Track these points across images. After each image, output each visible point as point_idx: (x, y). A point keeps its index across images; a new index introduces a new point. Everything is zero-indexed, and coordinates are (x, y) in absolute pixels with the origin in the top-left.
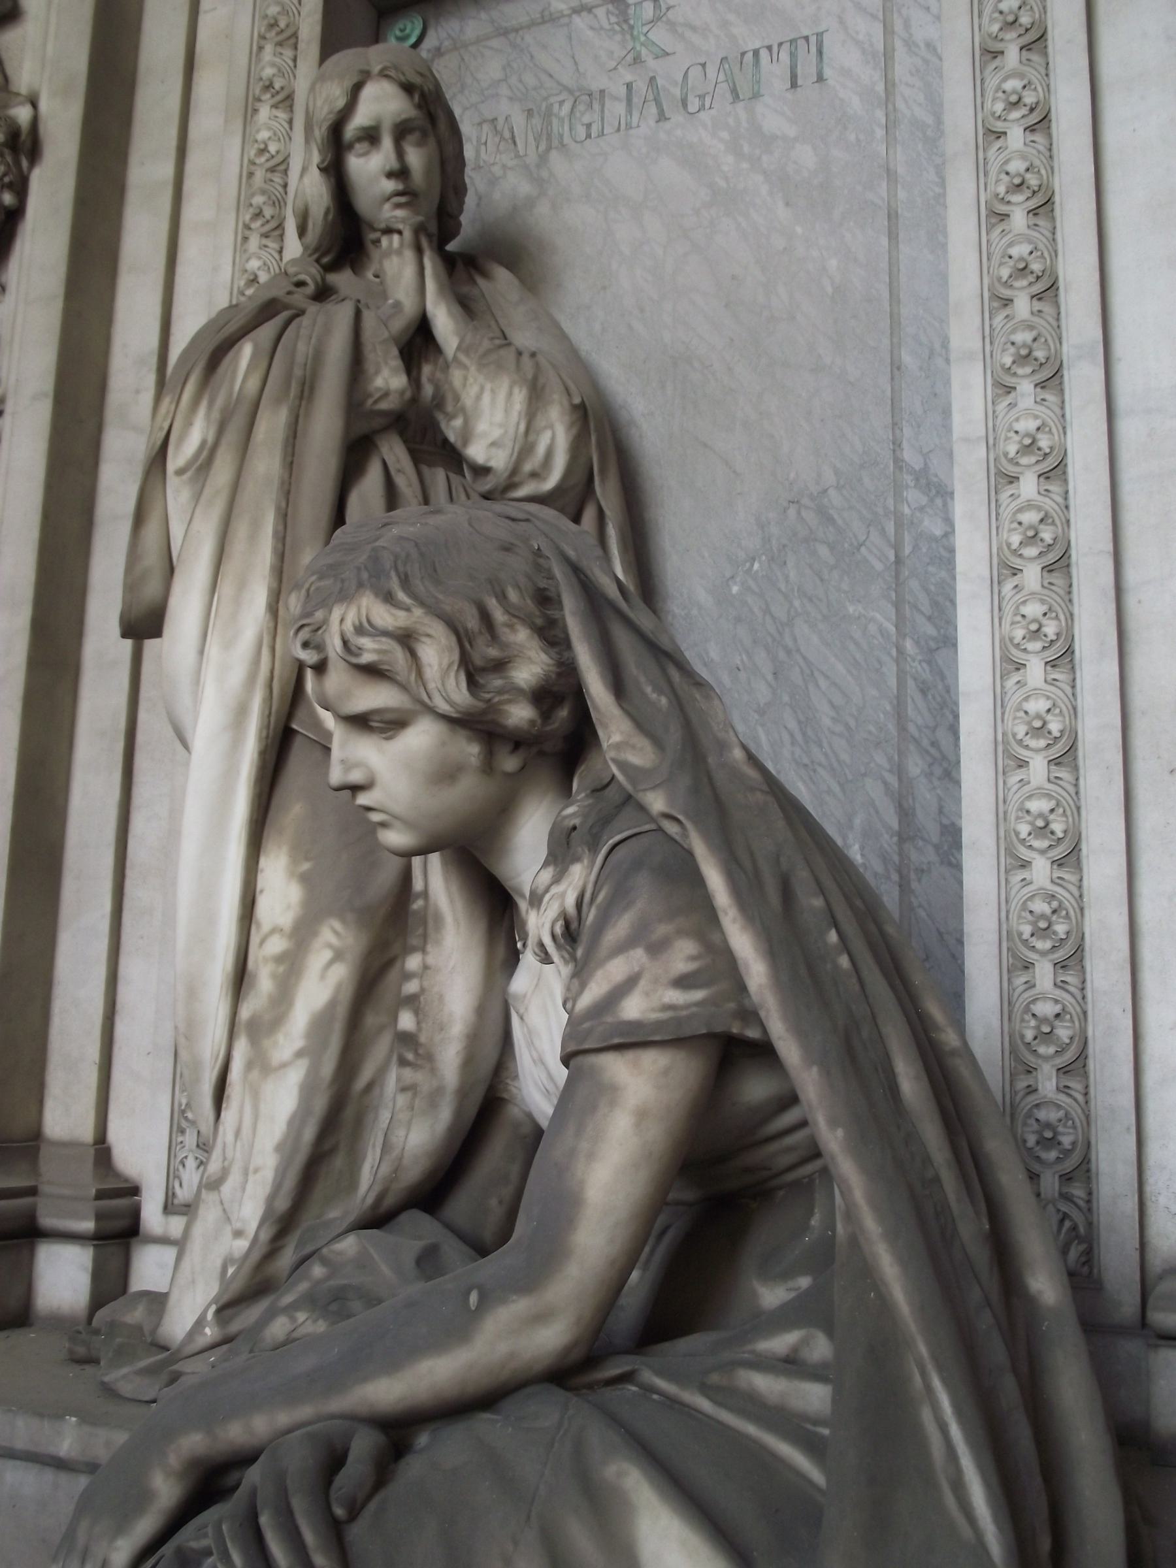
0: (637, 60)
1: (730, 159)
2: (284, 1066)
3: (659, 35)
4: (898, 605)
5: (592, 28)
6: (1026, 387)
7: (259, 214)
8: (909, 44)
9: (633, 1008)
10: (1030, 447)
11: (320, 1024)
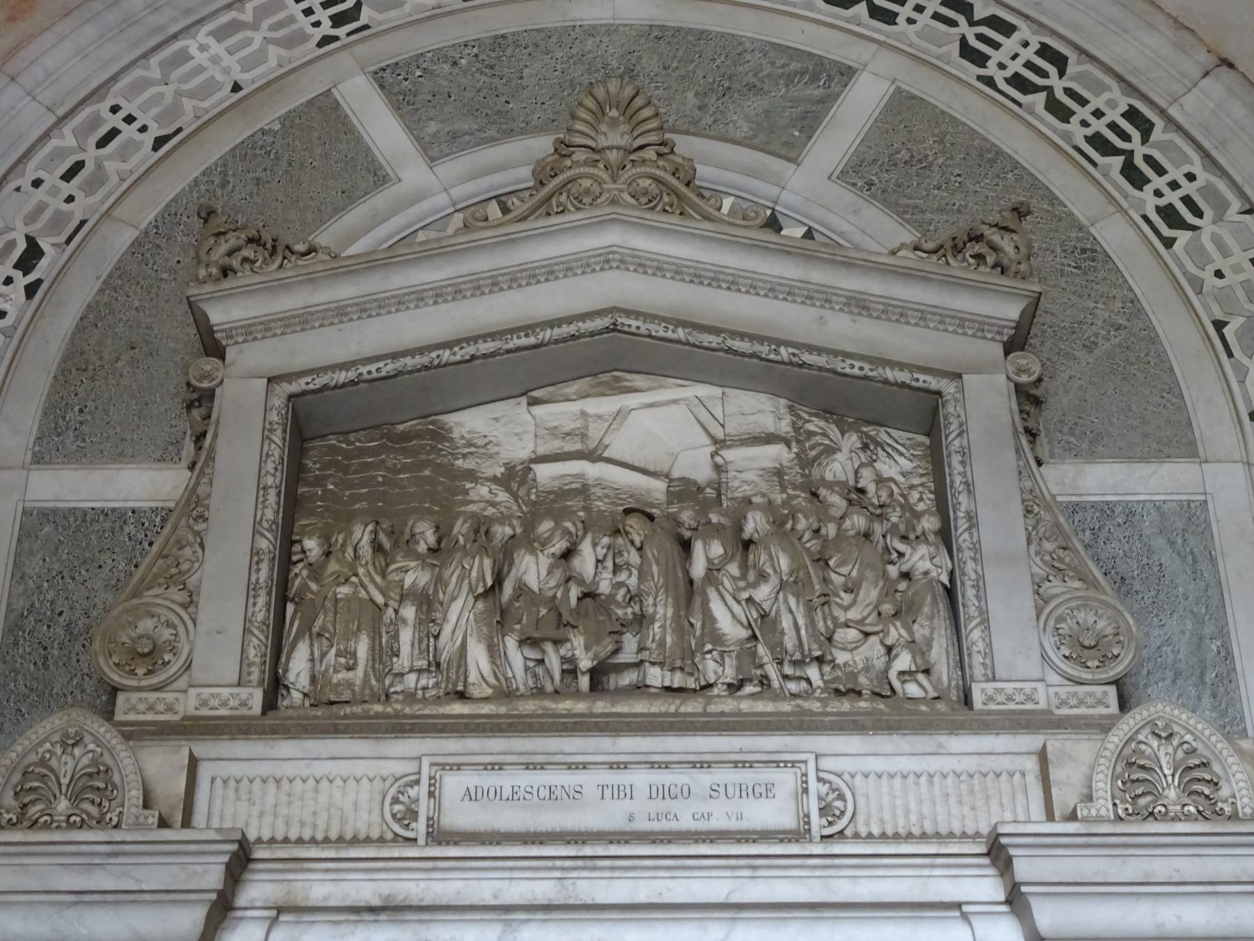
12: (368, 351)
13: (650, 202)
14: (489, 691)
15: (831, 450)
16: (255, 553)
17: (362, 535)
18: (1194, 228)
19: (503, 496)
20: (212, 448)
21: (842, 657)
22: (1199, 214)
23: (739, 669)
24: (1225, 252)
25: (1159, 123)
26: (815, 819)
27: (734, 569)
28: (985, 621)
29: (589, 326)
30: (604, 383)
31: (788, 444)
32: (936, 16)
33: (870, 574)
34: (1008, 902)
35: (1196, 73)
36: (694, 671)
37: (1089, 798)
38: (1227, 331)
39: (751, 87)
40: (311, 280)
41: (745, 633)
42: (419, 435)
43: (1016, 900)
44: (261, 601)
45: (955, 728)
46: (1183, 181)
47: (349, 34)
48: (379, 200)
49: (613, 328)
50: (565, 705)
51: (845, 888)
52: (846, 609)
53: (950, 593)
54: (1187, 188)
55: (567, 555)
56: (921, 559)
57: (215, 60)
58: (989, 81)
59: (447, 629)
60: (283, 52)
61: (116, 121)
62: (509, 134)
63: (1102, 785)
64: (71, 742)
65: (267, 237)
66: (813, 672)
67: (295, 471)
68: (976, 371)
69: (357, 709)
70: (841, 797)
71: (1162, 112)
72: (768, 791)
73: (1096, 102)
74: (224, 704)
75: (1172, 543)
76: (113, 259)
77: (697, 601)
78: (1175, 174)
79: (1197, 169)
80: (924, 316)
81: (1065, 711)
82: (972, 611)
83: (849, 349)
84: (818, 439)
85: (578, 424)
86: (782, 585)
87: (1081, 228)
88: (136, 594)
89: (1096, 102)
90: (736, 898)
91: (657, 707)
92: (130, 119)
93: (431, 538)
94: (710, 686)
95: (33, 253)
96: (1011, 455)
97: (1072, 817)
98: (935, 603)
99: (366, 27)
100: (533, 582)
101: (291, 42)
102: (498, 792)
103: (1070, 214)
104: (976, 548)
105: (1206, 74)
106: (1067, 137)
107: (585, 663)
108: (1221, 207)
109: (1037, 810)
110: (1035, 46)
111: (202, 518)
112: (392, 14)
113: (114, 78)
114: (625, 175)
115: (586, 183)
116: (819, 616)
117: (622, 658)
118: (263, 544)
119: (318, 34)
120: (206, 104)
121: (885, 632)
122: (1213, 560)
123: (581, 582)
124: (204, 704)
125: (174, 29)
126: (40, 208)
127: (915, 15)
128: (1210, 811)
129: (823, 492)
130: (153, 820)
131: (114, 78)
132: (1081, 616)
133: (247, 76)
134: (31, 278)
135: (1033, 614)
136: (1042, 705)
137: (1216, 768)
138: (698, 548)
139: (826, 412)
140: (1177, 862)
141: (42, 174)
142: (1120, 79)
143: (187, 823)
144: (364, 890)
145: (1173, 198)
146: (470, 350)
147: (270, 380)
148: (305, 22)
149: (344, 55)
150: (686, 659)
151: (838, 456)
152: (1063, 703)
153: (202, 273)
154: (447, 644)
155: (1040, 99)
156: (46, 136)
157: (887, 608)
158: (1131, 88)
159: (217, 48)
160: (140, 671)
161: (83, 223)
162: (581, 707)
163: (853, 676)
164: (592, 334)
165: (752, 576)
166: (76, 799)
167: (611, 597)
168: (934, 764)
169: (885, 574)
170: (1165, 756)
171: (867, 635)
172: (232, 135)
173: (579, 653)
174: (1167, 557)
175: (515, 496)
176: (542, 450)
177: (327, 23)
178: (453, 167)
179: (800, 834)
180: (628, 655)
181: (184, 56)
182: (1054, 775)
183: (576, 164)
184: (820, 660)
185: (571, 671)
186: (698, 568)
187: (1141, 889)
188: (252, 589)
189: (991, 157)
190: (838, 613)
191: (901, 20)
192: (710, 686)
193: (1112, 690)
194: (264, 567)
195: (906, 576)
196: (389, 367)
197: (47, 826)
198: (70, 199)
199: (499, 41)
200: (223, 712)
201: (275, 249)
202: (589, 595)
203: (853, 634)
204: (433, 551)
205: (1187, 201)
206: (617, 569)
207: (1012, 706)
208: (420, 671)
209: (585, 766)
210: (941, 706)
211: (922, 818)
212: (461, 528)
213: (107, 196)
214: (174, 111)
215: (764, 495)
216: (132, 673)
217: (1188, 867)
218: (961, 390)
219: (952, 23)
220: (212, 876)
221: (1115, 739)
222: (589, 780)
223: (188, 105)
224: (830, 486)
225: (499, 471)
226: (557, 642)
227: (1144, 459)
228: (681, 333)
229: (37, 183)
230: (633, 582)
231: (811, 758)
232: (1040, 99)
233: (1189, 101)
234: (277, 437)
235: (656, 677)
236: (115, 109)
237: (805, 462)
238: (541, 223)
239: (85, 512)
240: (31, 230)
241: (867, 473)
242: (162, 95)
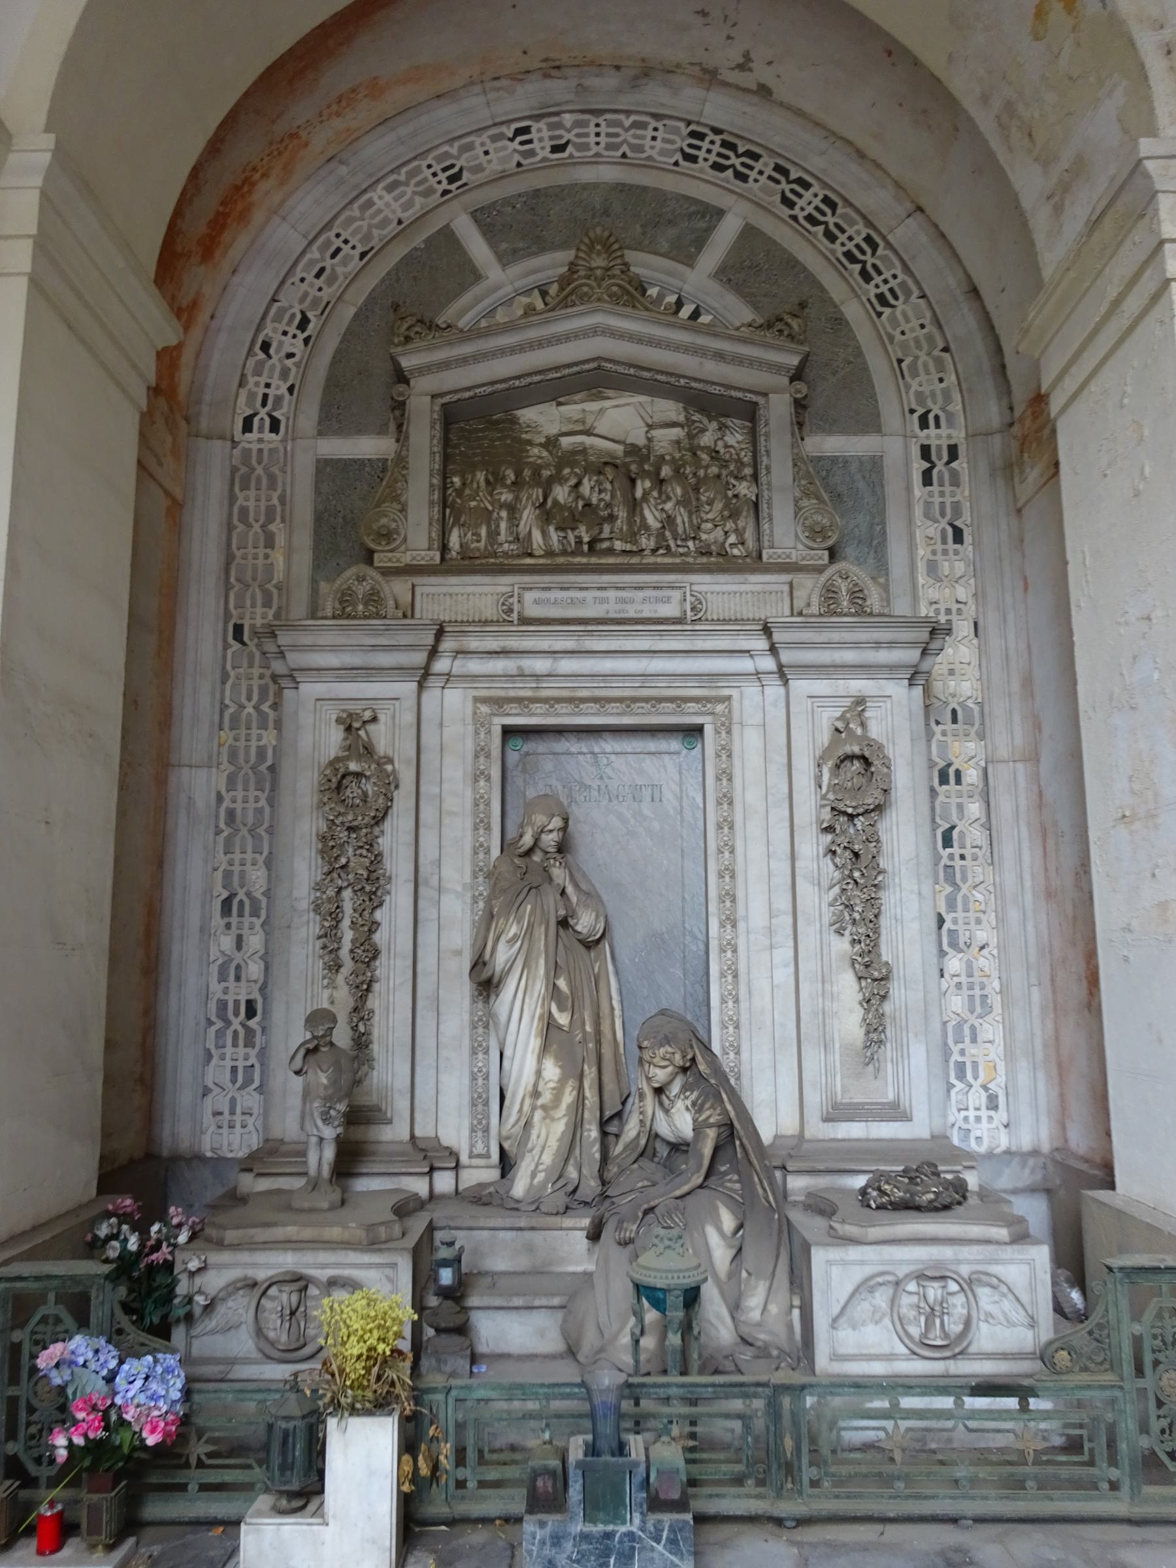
0: (601, 778)
3: (608, 771)
4: (684, 970)
6: (729, 927)
7: (482, 821)
8: (687, 795)
9: (712, 1120)
10: (729, 944)
11: (568, 1107)
12: (479, 381)
13: (615, 299)
14: (542, 553)
15: (703, 430)
16: (432, 485)
17: (481, 476)
18: (893, 306)
19: (545, 454)
20: (407, 431)
21: (704, 537)
22: (896, 298)
23: (657, 542)
24: (907, 321)
25: (882, 244)
26: (689, 613)
27: (655, 494)
28: (771, 520)
29: (587, 367)
30: (594, 395)
31: (682, 426)
32: (770, 178)
33: (719, 497)
34: (770, 650)
35: (904, 215)
36: (635, 542)
37: (808, 605)
38: (904, 365)
39: (670, 222)
40: (450, 344)
41: (659, 525)
42: (503, 421)
43: (773, 650)
44: (436, 509)
45: (753, 571)
46: (890, 279)
47: (458, 188)
48: (477, 290)
49: (599, 368)
50: (577, 560)
51: (700, 644)
52: (707, 513)
53: (756, 505)
54: (893, 283)
55: (578, 485)
56: (744, 489)
57: (388, 205)
58: (794, 218)
59: (522, 523)
60: (423, 200)
61: (338, 243)
62: (543, 250)
63: (815, 600)
64: (361, 579)
65: (427, 320)
66: (690, 544)
67: (446, 442)
68: (775, 392)
69: (483, 561)
70: (701, 603)
71: (884, 238)
72: (668, 600)
73: (850, 231)
74: (423, 559)
75: (864, 477)
76: (346, 323)
77: (638, 509)
78: (887, 275)
79: (898, 271)
80: (752, 362)
81: (804, 562)
82: (765, 515)
83: (715, 380)
84: (697, 424)
85: (581, 416)
86: (678, 503)
87: (835, 306)
88: (378, 505)
89: (850, 231)
90: (653, 648)
91: (619, 560)
92: (346, 242)
93: (512, 477)
94: (643, 550)
95: (303, 324)
96: (789, 436)
97: (800, 614)
98: (748, 510)
99: (465, 184)
100: (561, 500)
101: (429, 192)
102: (548, 600)
103: (831, 298)
104: (769, 484)
105: (909, 216)
106: (833, 252)
107: (586, 539)
108: (908, 293)
109: (787, 612)
110: (820, 197)
111: (404, 468)
112: (479, 175)
113: (335, 217)
114: (605, 284)
115: (585, 289)
116: (694, 517)
117: (603, 536)
118: (435, 481)
119: (440, 188)
120: (384, 232)
121: (724, 525)
122: (882, 486)
123: (583, 498)
124: (414, 559)
125: (364, 186)
126: (306, 294)
127: (758, 177)
128: (861, 612)
129: (699, 453)
130: (400, 615)
131: (335, 217)
132: (815, 517)
133: (406, 215)
134: (306, 334)
135: (793, 515)
136: (794, 560)
137: (866, 592)
138: (639, 483)
139: (702, 410)
140: (843, 634)
141: (304, 275)
142: (864, 217)
143: (413, 616)
144: (493, 644)
145: (884, 289)
146: (529, 380)
147: (433, 397)
148: (433, 181)
149: (455, 202)
150: (632, 537)
151: (707, 433)
152: (804, 559)
153: (396, 340)
154: (523, 529)
155: (820, 229)
156: (303, 253)
157: (726, 513)
158: (869, 224)
159: (388, 198)
160: (383, 543)
161: (328, 303)
162: (584, 560)
163: (709, 545)
164: (589, 371)
165: (664, 497)
166: (366, 604)
167: (598, 505)
168: (743, 588)
169: (726, 495)
170: (844, 586)
171: (716, 526)
172: (399, 252)
173: (583, 534)
174: (861, 485)
175: (550, 453)
176: (564, 429)
177: (445, 182)
178: (516, 269)
179: (680, 621)
180: (605, 534)
181: (370, 203)
182: (795, 594)
183: (580, 277)
184: (694, 538)
185: (579, 542)
186: (639, 493)
187: (827, 645)
188: (432, 503)
189: (792, 264)
190: (703, 515)
191: (751, 180)
192: (643, 550)
193: (826, 553)
194: (436, 492)
195: (736, 496)
196: (489, 389)
197: (354, 618)
198: (320, 289)
199: (537, 193)
200: (422, 563)
201: (432, 326)
202: (588, 505)
203: (710, 525)
204: (513, 483)
205: (891, 290)
206: (600, 491)
207: (780, 560)
208: (510, 542)
209: (587, 588)
210: (748, 560)
211: (736, 612)
212: (527, 473)
213: (340, 286)
214: (367, 237)
215: (670, 454)
216: (380, 544)
217: (847, 636)
218: (767, 402)
219: (778, 182)
220: (430, 640)
221: (823, 578)
222: (589, 595)
223: (376, 232)
224: (702, 448)
225: (543, 440)
226: (573, 529)
227: (855, 434)
228: (632, 371)
229: (302, 280)
230: (608, 498)
231: (688, 585)
232: (820, 229)
233: (899, 231)
234: (438, 427)
235: (618, 545)
236: (338, 236)
237: (690, 436)
238: (564, 312)
239: (345, 460)
240: (304, 306)
241: (720, 443)
242: (361, 227)
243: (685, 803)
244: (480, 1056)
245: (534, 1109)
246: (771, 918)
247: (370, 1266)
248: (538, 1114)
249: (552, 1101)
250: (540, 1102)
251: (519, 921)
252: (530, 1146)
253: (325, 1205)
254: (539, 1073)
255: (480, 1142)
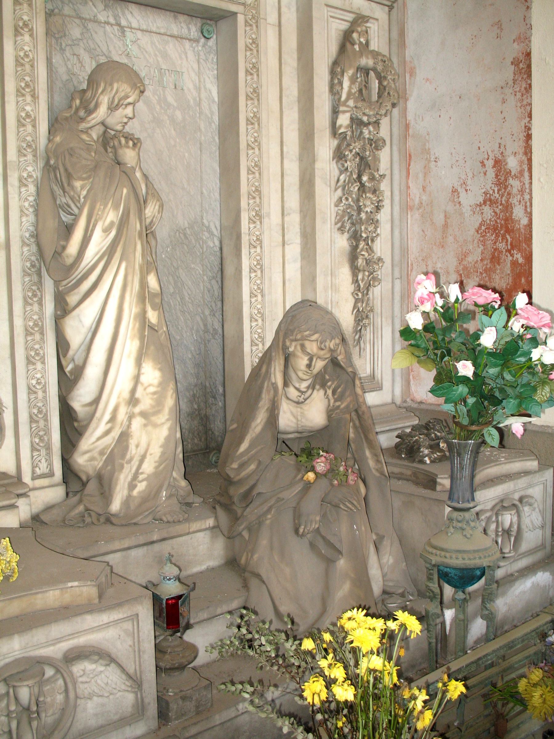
1: (158, 107)
2: (163, 424)
5: (113, 33)
11: (171, 410)
243: (203, 95)
244: (39, 366)
245: (131, 417)
246: (283, 214)
247: (107, 625)
248: (137, 423)
249: (153, 407)
250: (137, 410)
251: (116, 207)
252: (128, 457)
253: (287, 570)
254: (137, 379)
255: (43, 461)
